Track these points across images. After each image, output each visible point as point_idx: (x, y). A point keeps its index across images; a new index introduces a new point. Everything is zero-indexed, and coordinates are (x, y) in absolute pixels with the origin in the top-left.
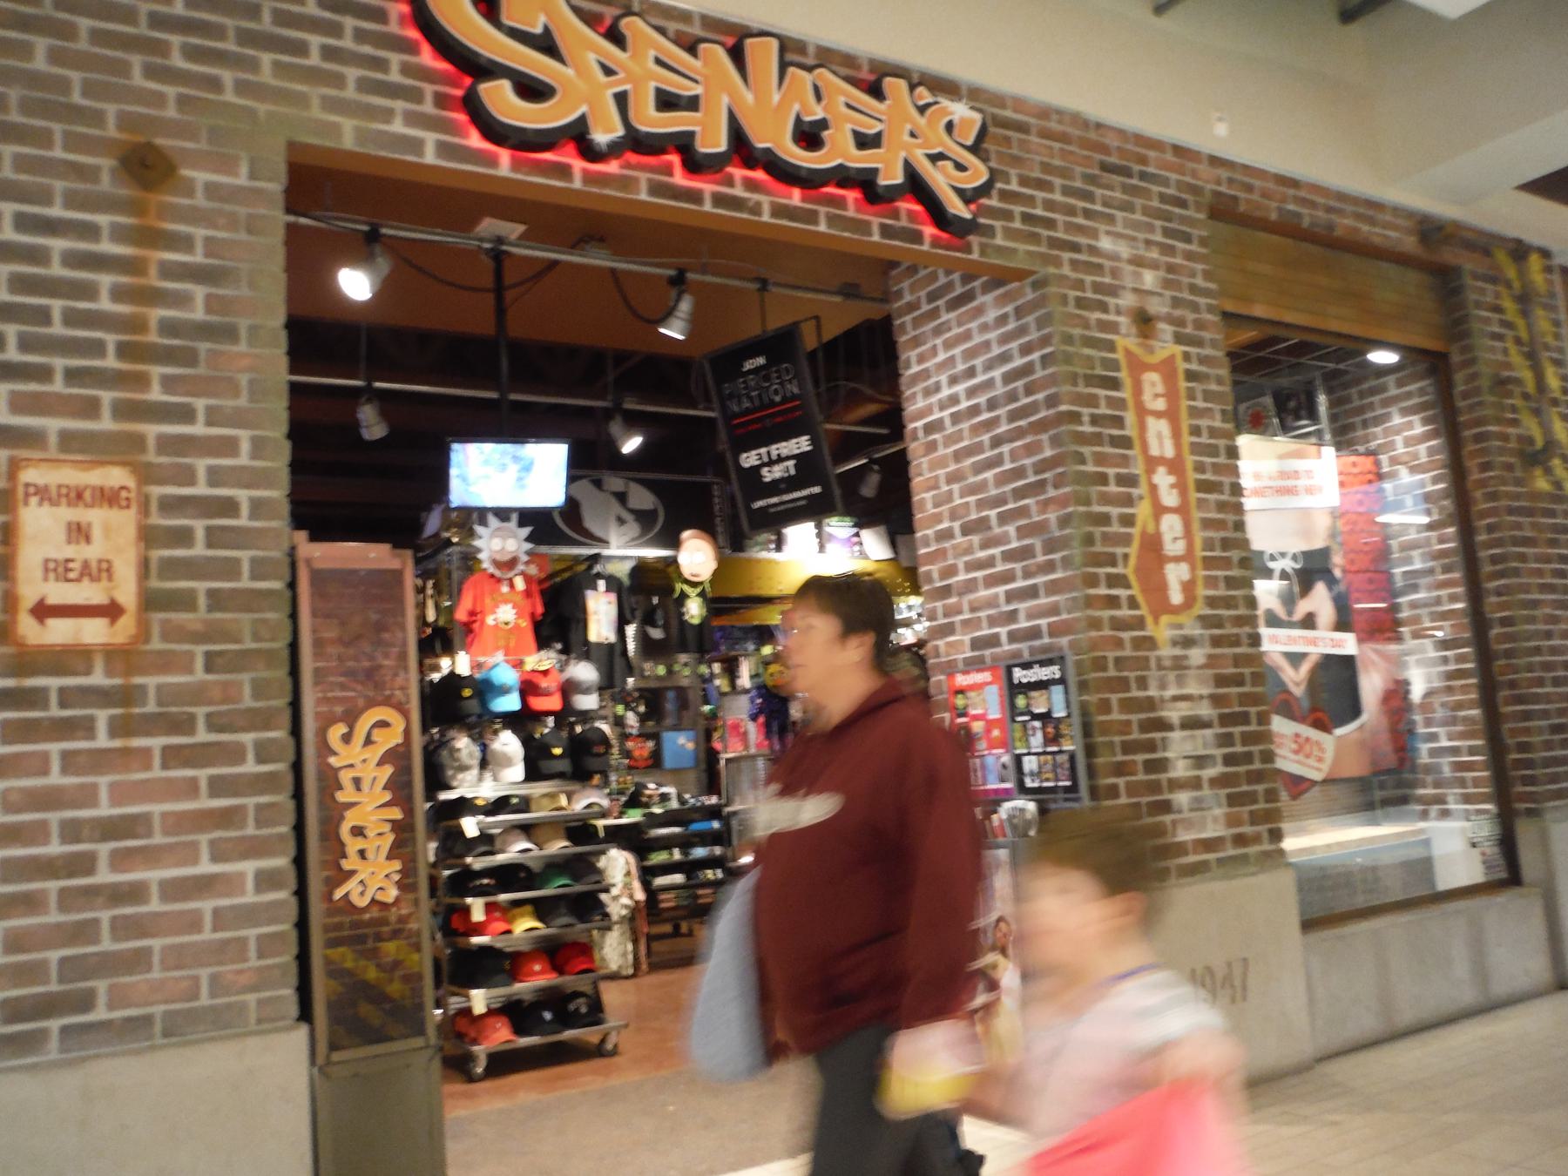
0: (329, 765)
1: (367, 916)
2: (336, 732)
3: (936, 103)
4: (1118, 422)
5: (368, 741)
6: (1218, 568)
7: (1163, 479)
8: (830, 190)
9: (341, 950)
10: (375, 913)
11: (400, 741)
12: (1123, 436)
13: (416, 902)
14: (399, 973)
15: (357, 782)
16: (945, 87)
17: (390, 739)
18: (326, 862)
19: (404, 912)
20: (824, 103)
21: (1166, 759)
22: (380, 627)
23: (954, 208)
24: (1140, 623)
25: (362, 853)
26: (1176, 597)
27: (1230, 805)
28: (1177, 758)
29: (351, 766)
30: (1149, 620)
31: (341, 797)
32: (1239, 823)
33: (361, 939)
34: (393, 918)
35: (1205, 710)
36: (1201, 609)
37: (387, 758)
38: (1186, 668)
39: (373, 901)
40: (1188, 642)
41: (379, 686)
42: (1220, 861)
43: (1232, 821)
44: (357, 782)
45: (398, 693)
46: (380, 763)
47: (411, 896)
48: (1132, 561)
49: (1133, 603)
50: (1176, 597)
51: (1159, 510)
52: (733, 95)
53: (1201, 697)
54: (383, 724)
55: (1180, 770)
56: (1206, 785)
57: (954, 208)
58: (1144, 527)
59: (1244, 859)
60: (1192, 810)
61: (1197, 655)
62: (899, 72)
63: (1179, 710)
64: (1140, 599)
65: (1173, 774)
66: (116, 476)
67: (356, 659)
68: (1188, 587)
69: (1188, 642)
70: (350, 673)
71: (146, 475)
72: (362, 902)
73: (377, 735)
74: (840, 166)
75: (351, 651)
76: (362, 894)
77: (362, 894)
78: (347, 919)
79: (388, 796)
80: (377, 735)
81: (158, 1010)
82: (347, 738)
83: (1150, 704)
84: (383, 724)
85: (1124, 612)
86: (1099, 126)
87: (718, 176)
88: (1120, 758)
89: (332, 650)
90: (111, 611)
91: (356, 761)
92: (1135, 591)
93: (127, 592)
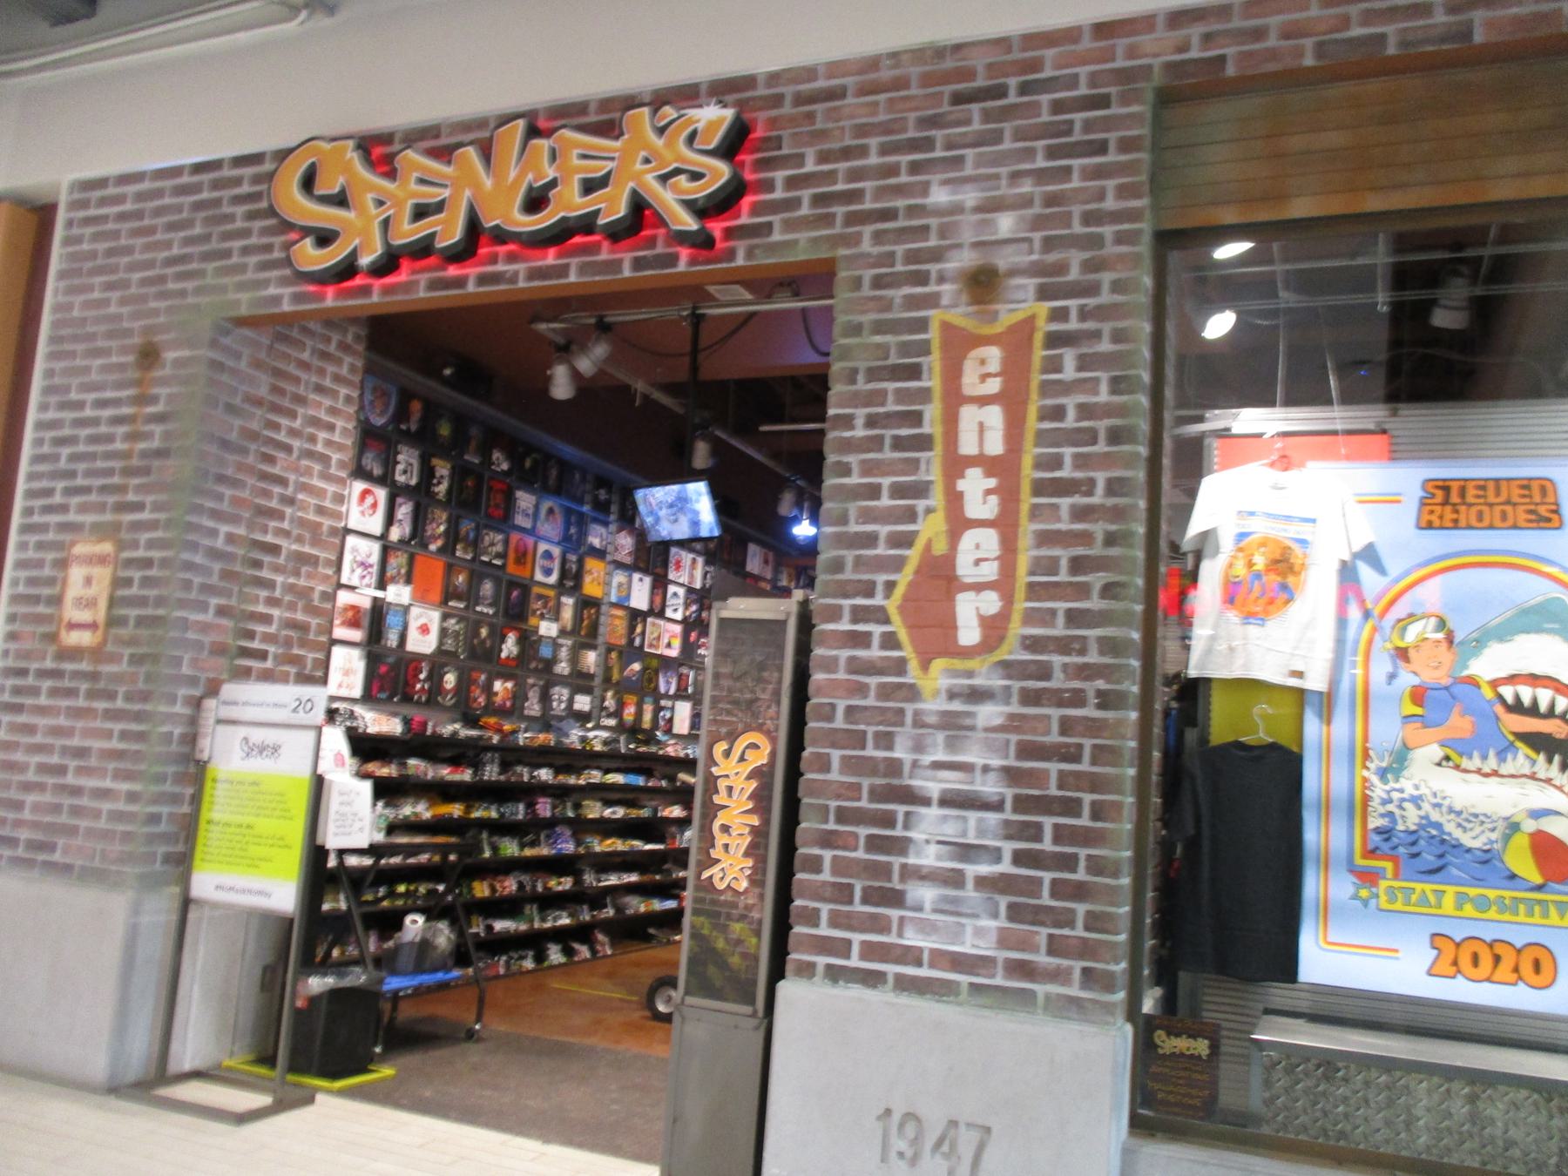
0: (711, 773)
1: (722, 898)
2: (721, 747)
3: (683, 116)
4: (916, 418)
5: (742, 759)
6: (1061, 599)
7: (976, 490)
8: (577, 239)
9: (702, 919)
10: (728, 897)
11: (765, 762)
12: (921, 435)
13: (761, 897)
14: (739, 949)
15: (730, 789)
16: (687, 95)
17: (759, 759)
18: (548, 837)
19: (750, 901)
20: (558, 161)
21: (908, 840)
22: (762, 667)
23: (680, 224)
24: (900, 666)
25: (726, 846)
26: (969, 634)
27: (1011, 918)
28: (928, 842)
29: (727, 776)
30: (913, 665)
31: (717, 800)
32: (1025, 944)
33: (718, 915)
34: (741, 905)
35: (990, 787)
36: (1010, 651)
37: (755, 774)
38: (972, 728)
39: (729, 886)
40: (977, 695)
41: (755, 715)
42: (974, 987)
43: (1004, 940)
44: (730, 789)
45: (769, 722)
46: (749, 778)
47: (757, 890)
48: (899, 591)
49: (890, 641)
50: (969, 634)
51: (959, 523)
52: (477, 186)
53: (986, 769)
54: (754, 746)
55: (929, 857)
56: (970, 884)
57: (681, 223)
58: (928, 546)
59: (1027, 998)
60: (935, 911)
61: (989, 714)
62: (630, 102)
63: (941, 781)
64: (903, 636)
65: (912, 860)
66: (107, 548)
67: (741, 691)
68: (994, 628)
69: (977, 695)
70: (736, 702)
71: (121, 546)
72: (721, 886)
73: (749, 755)
74: (564, 219)
75: (738, 685)
76: (722, 878)
77: (722, 878)
78: (709, 897)
79: (750, 806)
80: (749, 755)
81: (79, 862)
82: (727, 754)
83: (894, 767)
84: (754, 746)
85: (875, 652)
86: (958, 48)
87: (476, 259)
88: (831, 826)
89: (725, 683)
90: (93, 626)
91: (732, 773)
92: (898, 626)
93: (101, 614)
